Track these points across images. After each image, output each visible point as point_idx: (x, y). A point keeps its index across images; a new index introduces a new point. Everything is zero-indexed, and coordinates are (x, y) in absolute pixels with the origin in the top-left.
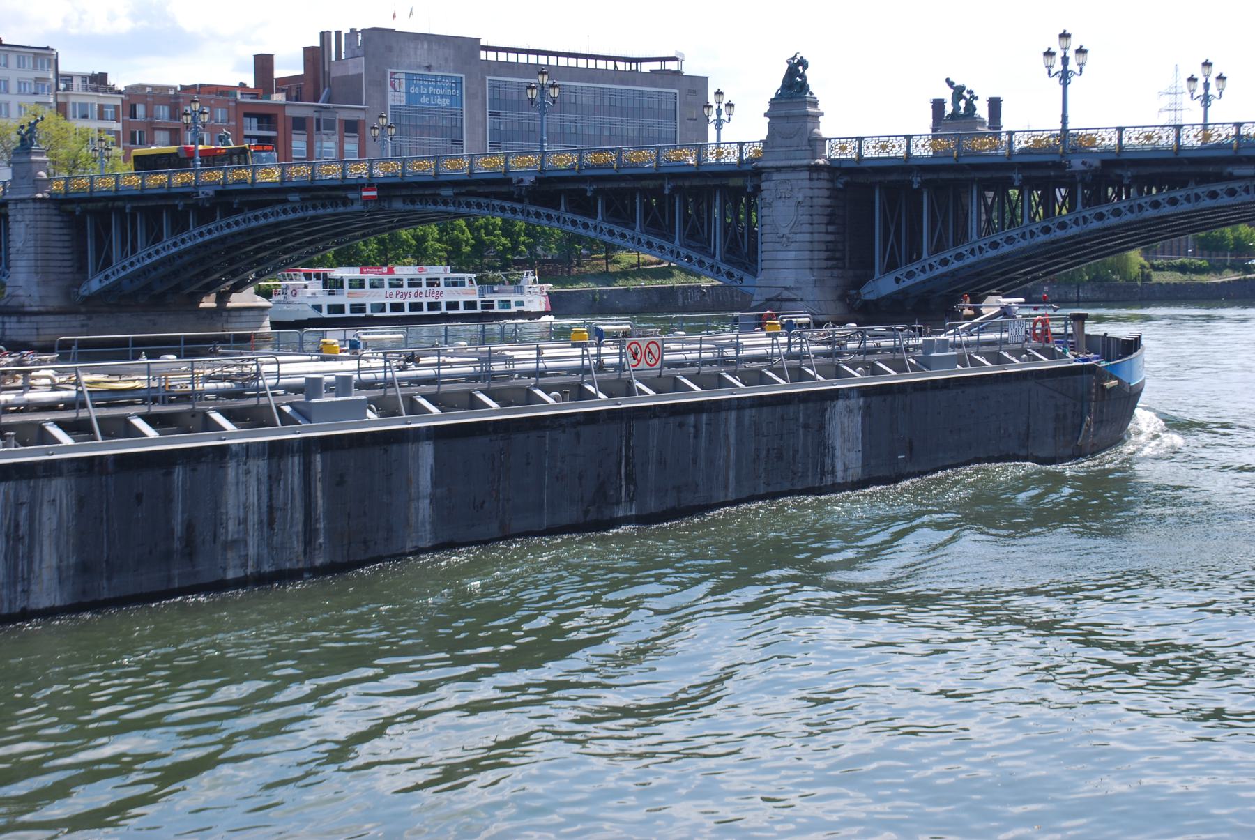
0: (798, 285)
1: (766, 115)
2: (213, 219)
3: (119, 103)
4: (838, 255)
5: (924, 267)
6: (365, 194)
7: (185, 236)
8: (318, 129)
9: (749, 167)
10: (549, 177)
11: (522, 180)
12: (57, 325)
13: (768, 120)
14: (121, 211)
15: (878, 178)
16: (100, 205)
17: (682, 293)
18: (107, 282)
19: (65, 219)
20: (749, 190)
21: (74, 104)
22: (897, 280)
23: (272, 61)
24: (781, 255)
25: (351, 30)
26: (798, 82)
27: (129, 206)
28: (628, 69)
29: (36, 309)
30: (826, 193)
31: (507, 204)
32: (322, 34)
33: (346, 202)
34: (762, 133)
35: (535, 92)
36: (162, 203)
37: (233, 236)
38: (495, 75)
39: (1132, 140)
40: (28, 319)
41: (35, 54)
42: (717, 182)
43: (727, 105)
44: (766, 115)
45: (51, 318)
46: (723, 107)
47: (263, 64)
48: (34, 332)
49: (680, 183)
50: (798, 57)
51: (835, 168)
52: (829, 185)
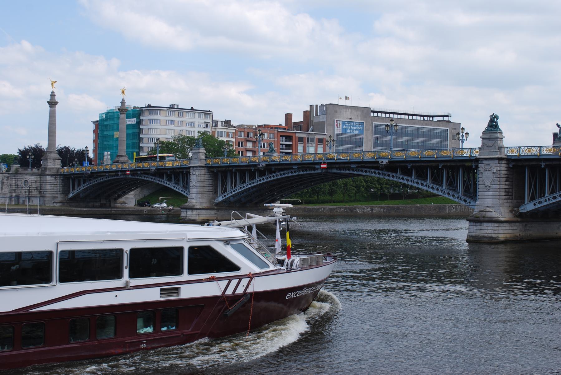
0: (493, 206)
1: (481, 137)
2: (265, 175)
3: (234, 131)
4: (510, 194)
5: (546, 200)
6: (322, 166)
7: (254, 181)
8: (308, 142)
9: (473, 158)
10: (393, 161)
11: (383, 162)
12: (206, 213)
13: (482, 139)
14: (231, 171)
15: (527, 163)
16: (224, 169)
17: (448, 207)
18: (225, 198)
19: (211, 174)
20: (474, 167)
21: (218, 131)
22: (535, 205)
23: (292, 116)
24: (486, 193)
25: (322, 104)
26: (494, 125)
27: (234, 169)
28: (429, 120)
29: (198, 207)
30: (505, 169)
31: (377, 171)
32: (311, 106)
33: (315, 169)
34: (479, 145)
35: (389, 127)
36: (245, 168)
37: (272, 181)
38: (376, 122)
39: (524, 153)
40: (195, 211)
41: (205, 113)
42: (461, 164)
43: (466, 134)
44: (481, 137)
45: (204, 211)
46: (464, 134)
47: (288, 117)
48: (198, 216)
49: (446, 164)
50: (495, 114)
51: (509, 160)
52: (507, 166)
